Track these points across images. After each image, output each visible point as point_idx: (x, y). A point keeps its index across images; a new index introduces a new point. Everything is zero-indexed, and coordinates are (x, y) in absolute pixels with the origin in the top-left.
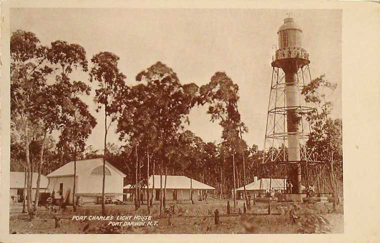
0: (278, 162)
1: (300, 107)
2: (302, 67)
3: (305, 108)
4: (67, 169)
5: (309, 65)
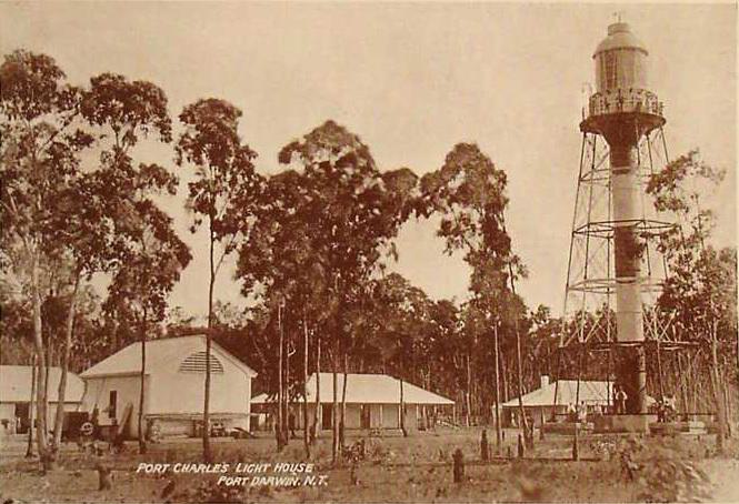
0: (593, 344)
1: (643, 221)
2: (648, 133)
3: (653, 225)
4: (125, 360)
5: (664, 127)
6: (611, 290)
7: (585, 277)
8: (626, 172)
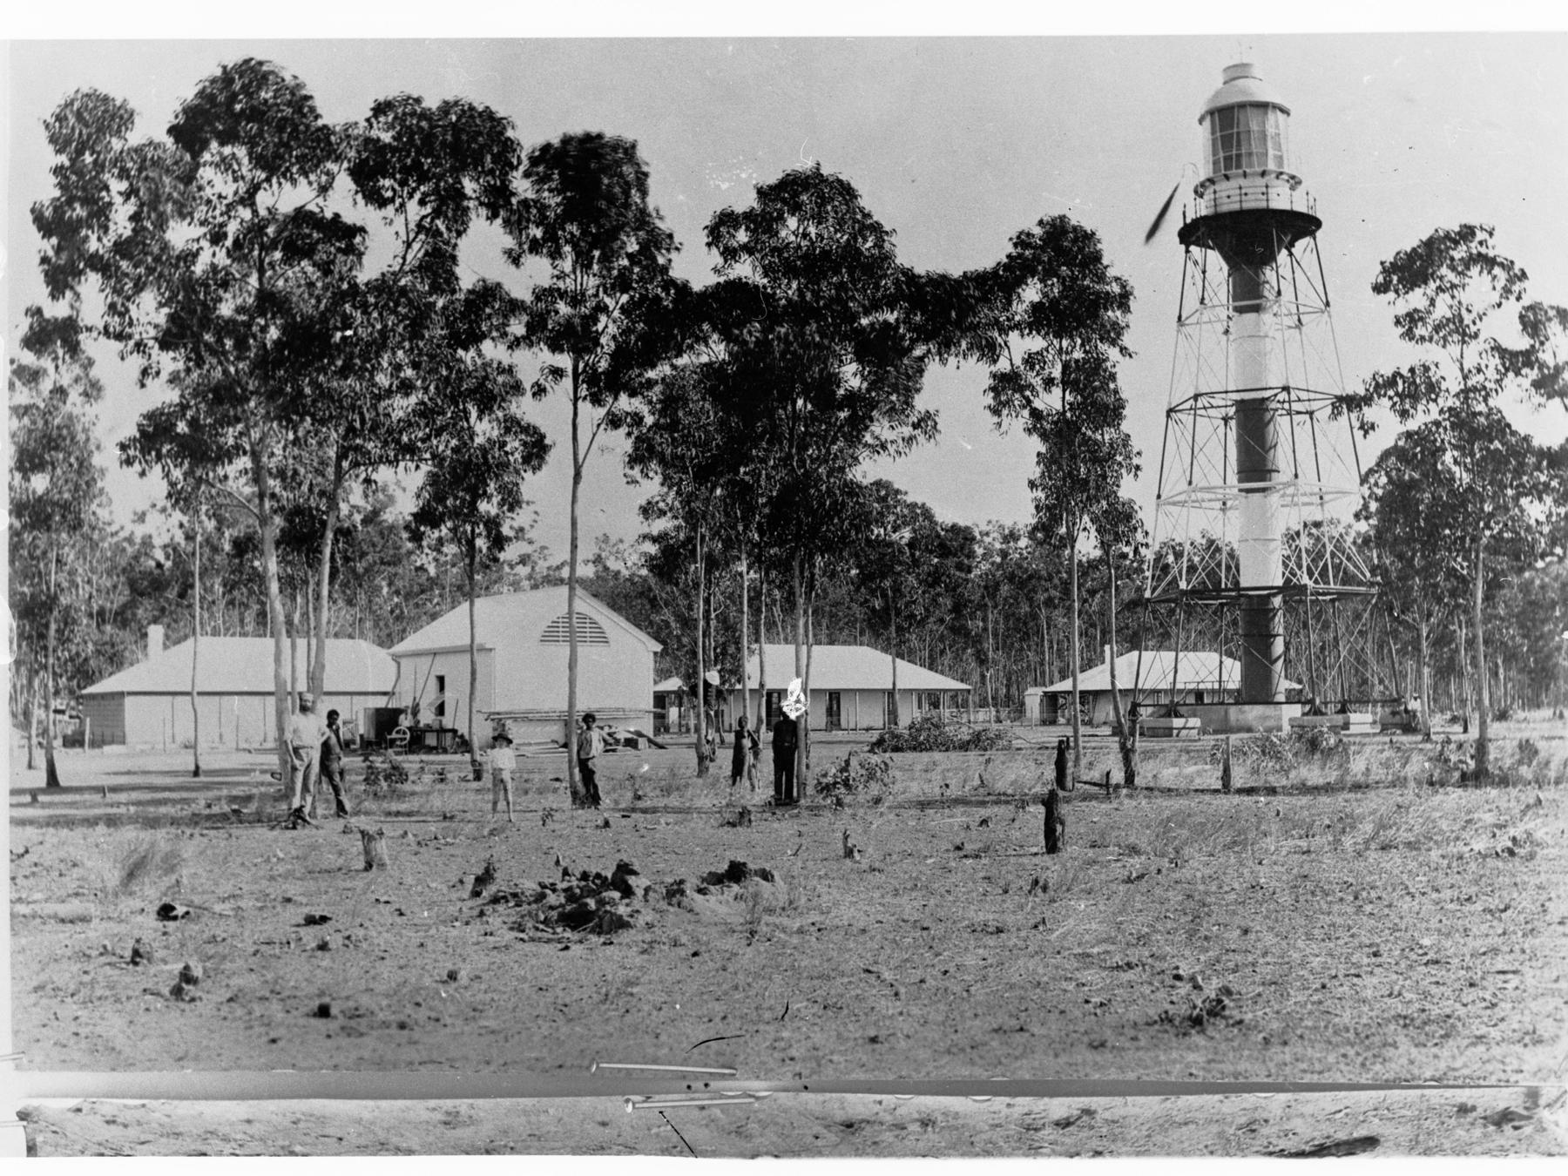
1: (1286, 389)
3: (1304, 395)
4: (449, 628)
5: (1319, 234)
6: (1229, 504)
7: (1190, 483)
8: (1257, 309)
